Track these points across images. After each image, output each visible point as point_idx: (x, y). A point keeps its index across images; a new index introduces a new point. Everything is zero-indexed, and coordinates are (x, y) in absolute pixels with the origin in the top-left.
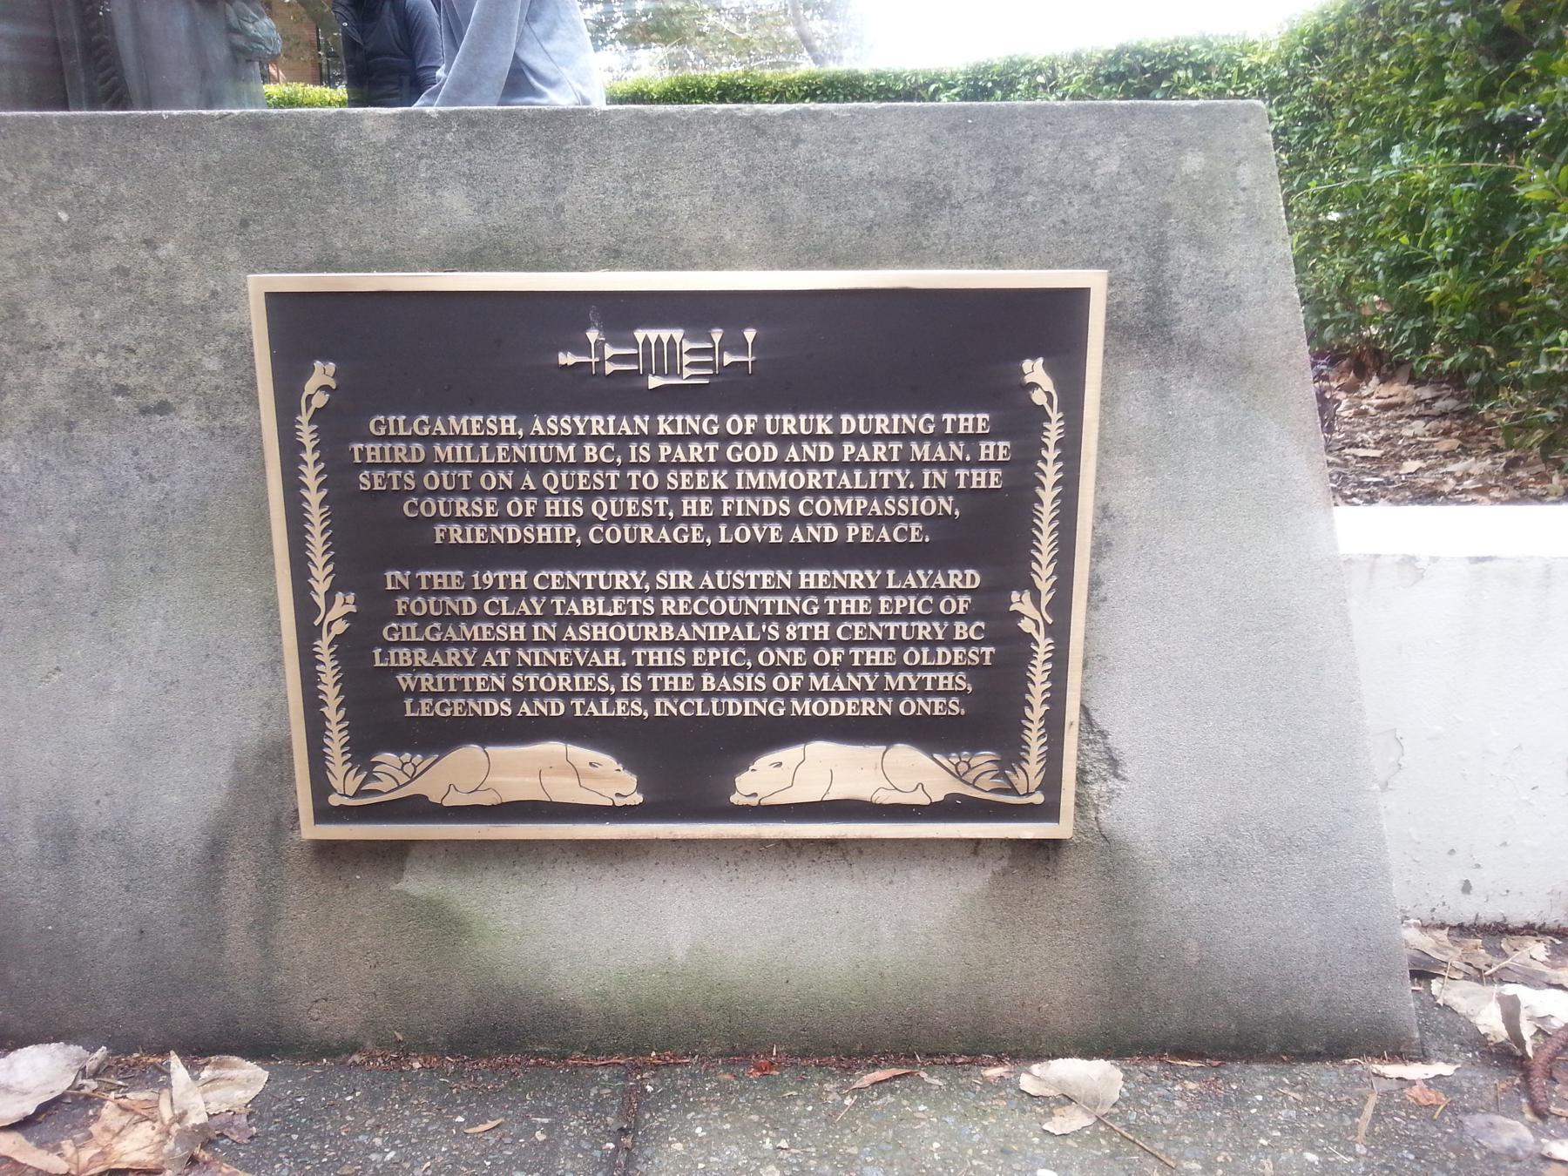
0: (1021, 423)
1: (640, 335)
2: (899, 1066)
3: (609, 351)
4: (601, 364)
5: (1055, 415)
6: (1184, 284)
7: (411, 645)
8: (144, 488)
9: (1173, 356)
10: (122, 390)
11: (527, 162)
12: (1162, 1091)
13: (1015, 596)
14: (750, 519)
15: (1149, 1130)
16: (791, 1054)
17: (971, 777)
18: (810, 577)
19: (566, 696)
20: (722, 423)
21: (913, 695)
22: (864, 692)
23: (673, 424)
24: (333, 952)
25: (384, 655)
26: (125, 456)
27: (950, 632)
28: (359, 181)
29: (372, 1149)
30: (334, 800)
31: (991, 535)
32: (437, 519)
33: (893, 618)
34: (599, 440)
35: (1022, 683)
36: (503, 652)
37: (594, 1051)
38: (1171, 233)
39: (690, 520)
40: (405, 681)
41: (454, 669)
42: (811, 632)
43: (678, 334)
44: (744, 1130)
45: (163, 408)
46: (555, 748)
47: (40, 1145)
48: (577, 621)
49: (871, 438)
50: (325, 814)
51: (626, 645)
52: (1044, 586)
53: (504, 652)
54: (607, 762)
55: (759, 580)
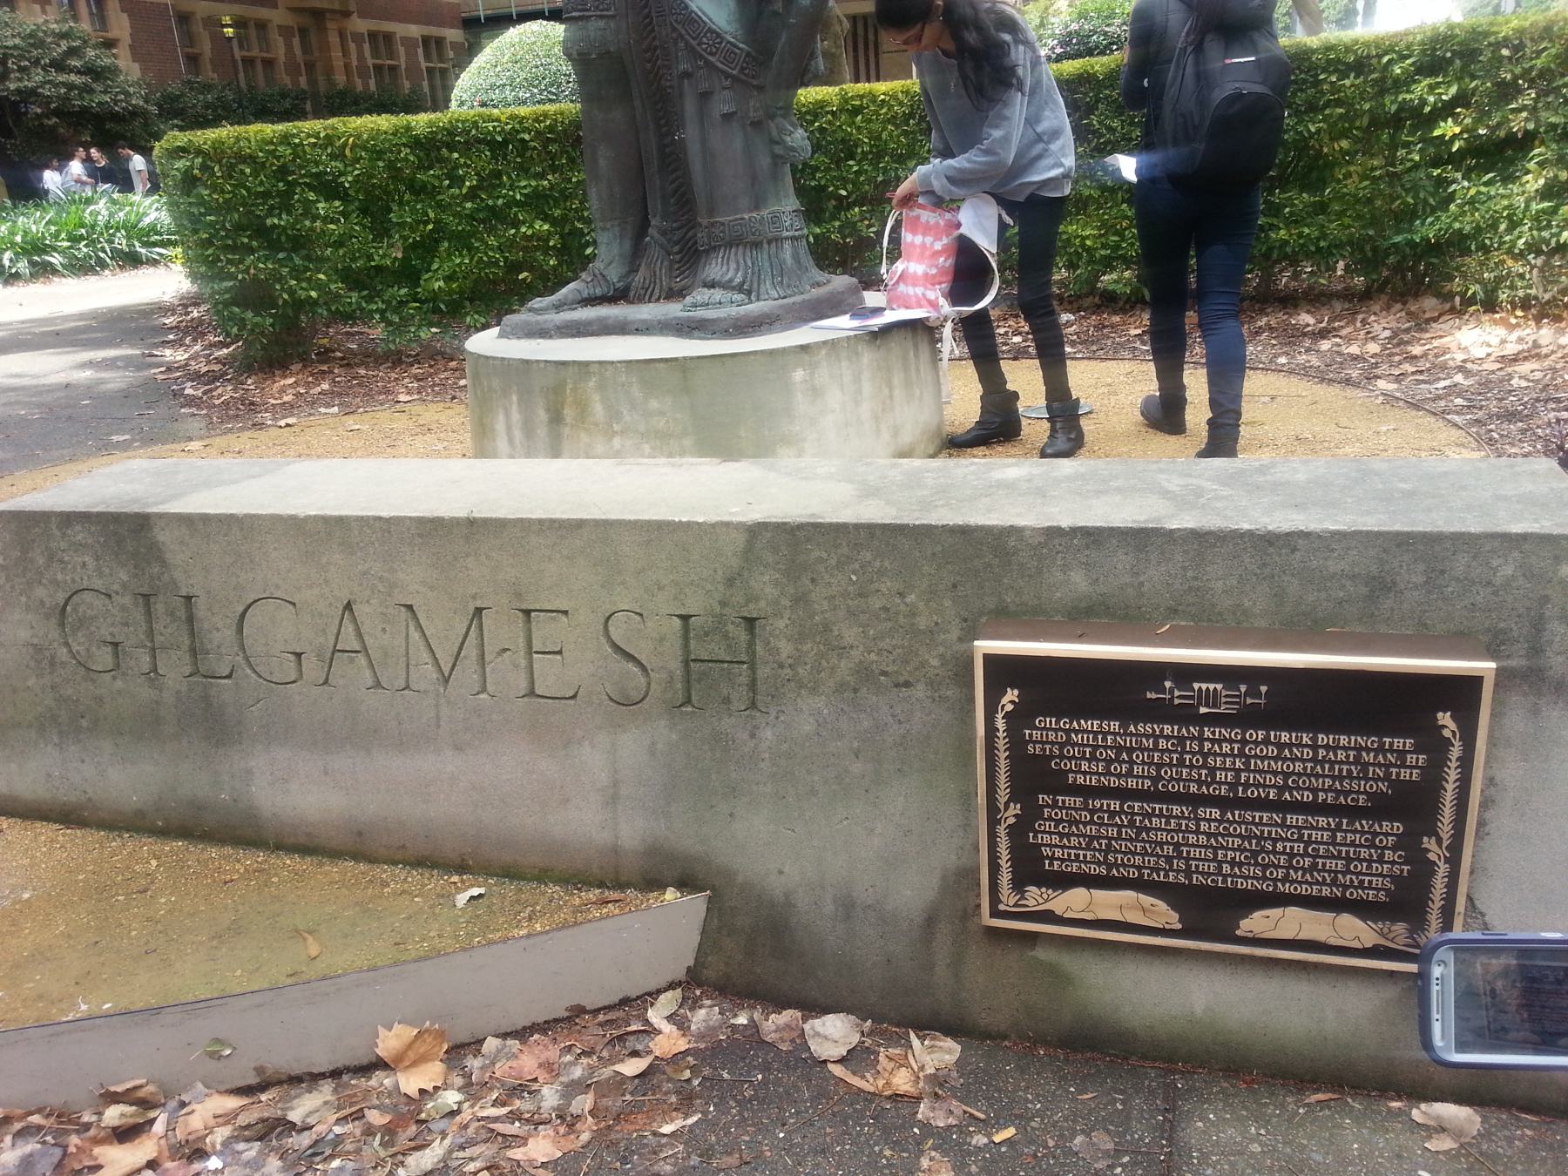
0: (1435, 747)
1: (1196, 686)
2: (1334, 1092)
3: (1177, 693)
4: (1172, 699)
5: (1457, 743)
6: (1555, 647)
7: (1050, 833)
8: (896, 727)
9: (1545, 690)
10: (884, 673)
11: (1123, 557)
12: (1507, 1133)
13: (1425, 839)
14: (1258, 785)
15: (1494, 1158)
16: (1265, 1075)
17: (1391, 936)
18: (1291, 819)
19: (1139, 868)
20: (1244, 734)
21: (1356, 888)
22: (1324, 883)
23: (1213, 733)
24: (991, 987)
25: (1035, 837)
26: (886, 709)
27: (1381, 856)
28: (1021, 565)
29: (1027, 1100)
30: (1002, 907)
31: (1413, 806)
32: (1071, 770)
33: (1345, 845)
34: (1168, 738)
35: (1428, 888)
36: (1104, 842)
37: (1144, 1057)
38: (1548, 614)
39: (1220, 783)
40: (1046, 851)
41: (1074, 848)
42: (1292, 848)
43: (1219, 687)
44: (1237, 1119)
45: (907, 684)
46: (1129, 895)
47: (854, 1073)
48: (1148, 830)
49: (1335, 749)
50: (995, 913)
51: (1177, 846)
52: (1445, 836)
53: (1104, 842)
54: (1162, 905)
55: (1261, 818)
